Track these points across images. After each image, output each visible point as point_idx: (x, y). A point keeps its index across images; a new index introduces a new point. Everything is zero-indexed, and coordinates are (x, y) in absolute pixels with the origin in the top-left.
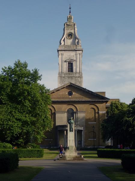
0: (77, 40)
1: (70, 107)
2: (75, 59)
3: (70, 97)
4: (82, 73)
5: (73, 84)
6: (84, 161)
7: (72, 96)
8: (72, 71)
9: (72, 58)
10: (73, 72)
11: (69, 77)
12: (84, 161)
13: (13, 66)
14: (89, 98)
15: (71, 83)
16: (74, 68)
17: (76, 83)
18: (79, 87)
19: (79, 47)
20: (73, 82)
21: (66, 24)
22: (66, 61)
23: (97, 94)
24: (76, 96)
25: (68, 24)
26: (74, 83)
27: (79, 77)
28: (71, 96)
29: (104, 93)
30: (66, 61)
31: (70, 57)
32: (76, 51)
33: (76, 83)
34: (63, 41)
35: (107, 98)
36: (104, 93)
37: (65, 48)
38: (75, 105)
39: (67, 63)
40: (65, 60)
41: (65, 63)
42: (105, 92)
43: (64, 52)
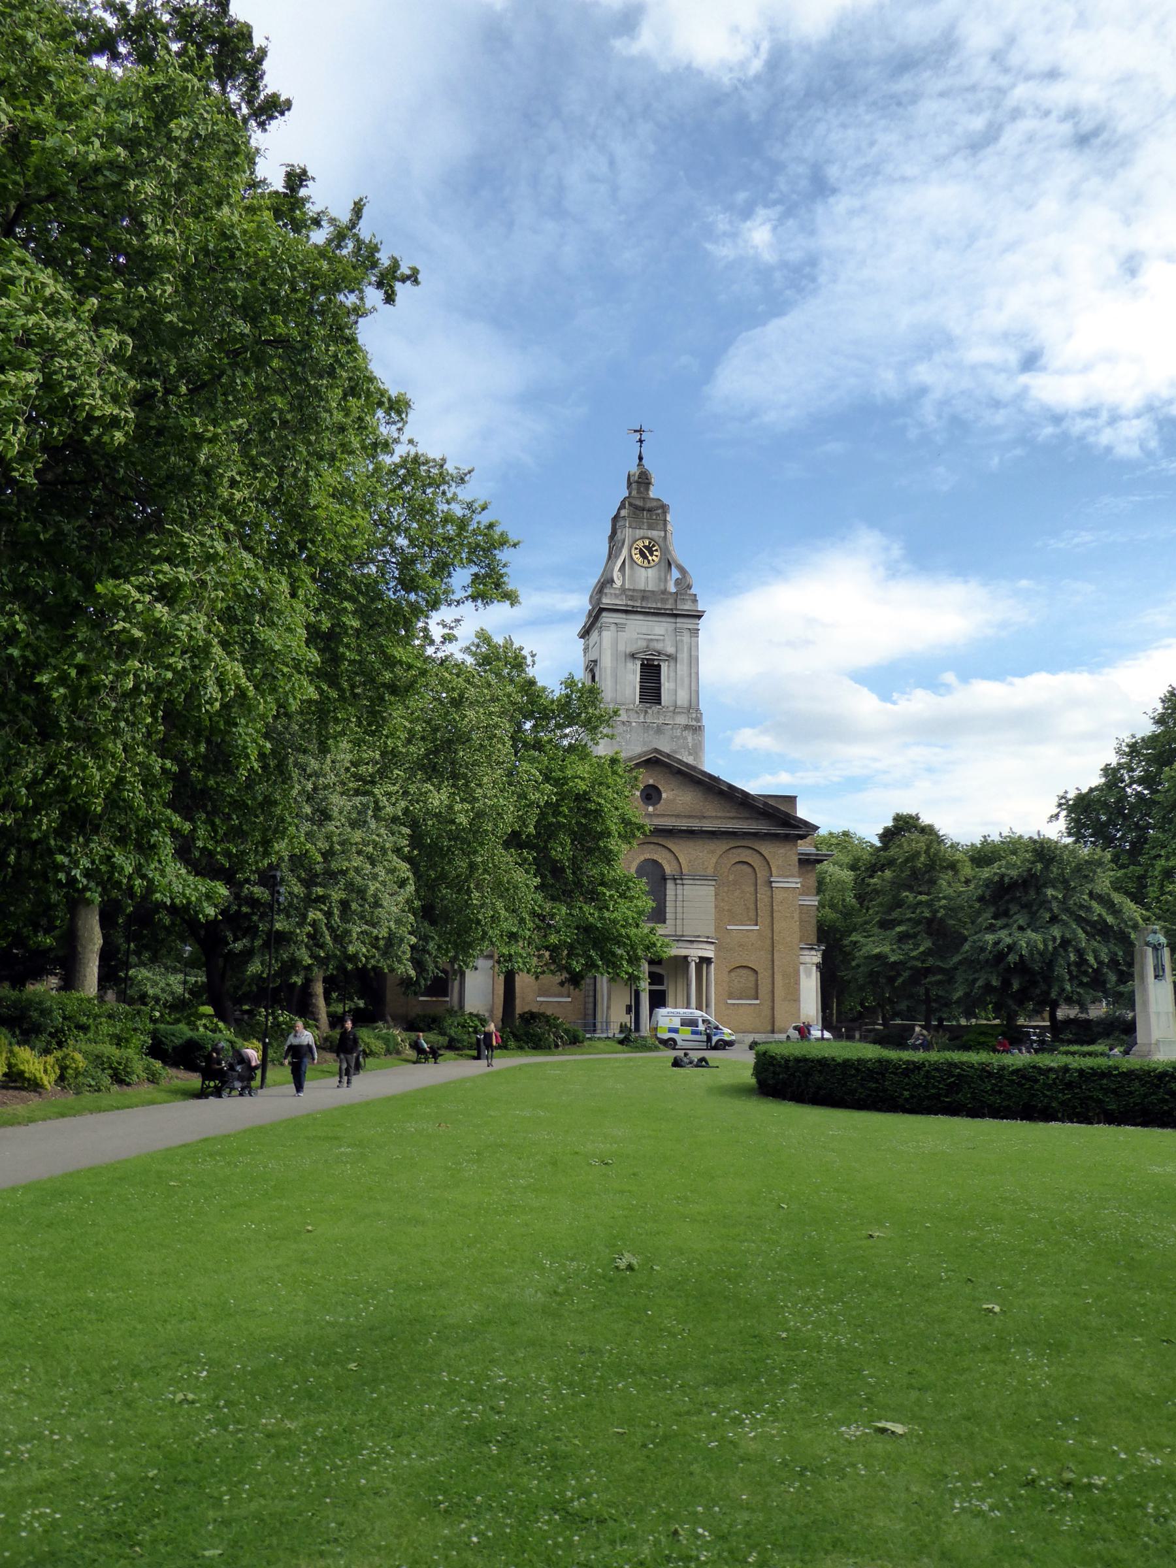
0: (675, 574)
1: (648, 856)
2: (670, 650)
3: (651, 809)
4: (698, 710)
5: (668, 756)
6: (609, 998)
7: (658, 806)
8: (657, 700)
9: (659, 646)
10: (660, 704)
11: (645, 726)
12: (609, 998)
13: (282, 98)
14: (92, 929)
15: (656, 750)
16: (666, 686)
17: (676, 752)
18: (694, 768)
19: (689, 602)
20: (665, 745)
21: (630, 504)
22: (633, 656)
23: (766, 804)
24: (677, 801)
25: (639, 503)
26: (667, 750)
27: (687, 727)
28: (653, 805)
29: (792, 800)
30: (633, 656)
31: (652, 640)
32: (676, 616)
33: (676, 752)
34: (620, 570)
35: (806, 824)
36: (792, 800)
37: (630, 603)
38: (670, 845)
39: (639, 663)
40: (631, 649)
41: (630, 665)
42: (795, 797)
43: (624, 616)
